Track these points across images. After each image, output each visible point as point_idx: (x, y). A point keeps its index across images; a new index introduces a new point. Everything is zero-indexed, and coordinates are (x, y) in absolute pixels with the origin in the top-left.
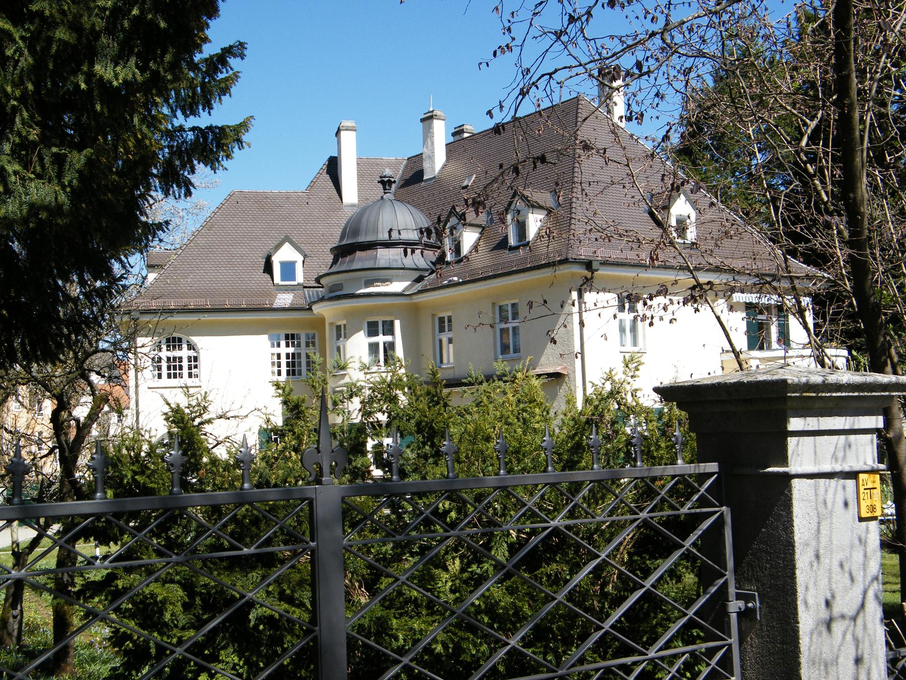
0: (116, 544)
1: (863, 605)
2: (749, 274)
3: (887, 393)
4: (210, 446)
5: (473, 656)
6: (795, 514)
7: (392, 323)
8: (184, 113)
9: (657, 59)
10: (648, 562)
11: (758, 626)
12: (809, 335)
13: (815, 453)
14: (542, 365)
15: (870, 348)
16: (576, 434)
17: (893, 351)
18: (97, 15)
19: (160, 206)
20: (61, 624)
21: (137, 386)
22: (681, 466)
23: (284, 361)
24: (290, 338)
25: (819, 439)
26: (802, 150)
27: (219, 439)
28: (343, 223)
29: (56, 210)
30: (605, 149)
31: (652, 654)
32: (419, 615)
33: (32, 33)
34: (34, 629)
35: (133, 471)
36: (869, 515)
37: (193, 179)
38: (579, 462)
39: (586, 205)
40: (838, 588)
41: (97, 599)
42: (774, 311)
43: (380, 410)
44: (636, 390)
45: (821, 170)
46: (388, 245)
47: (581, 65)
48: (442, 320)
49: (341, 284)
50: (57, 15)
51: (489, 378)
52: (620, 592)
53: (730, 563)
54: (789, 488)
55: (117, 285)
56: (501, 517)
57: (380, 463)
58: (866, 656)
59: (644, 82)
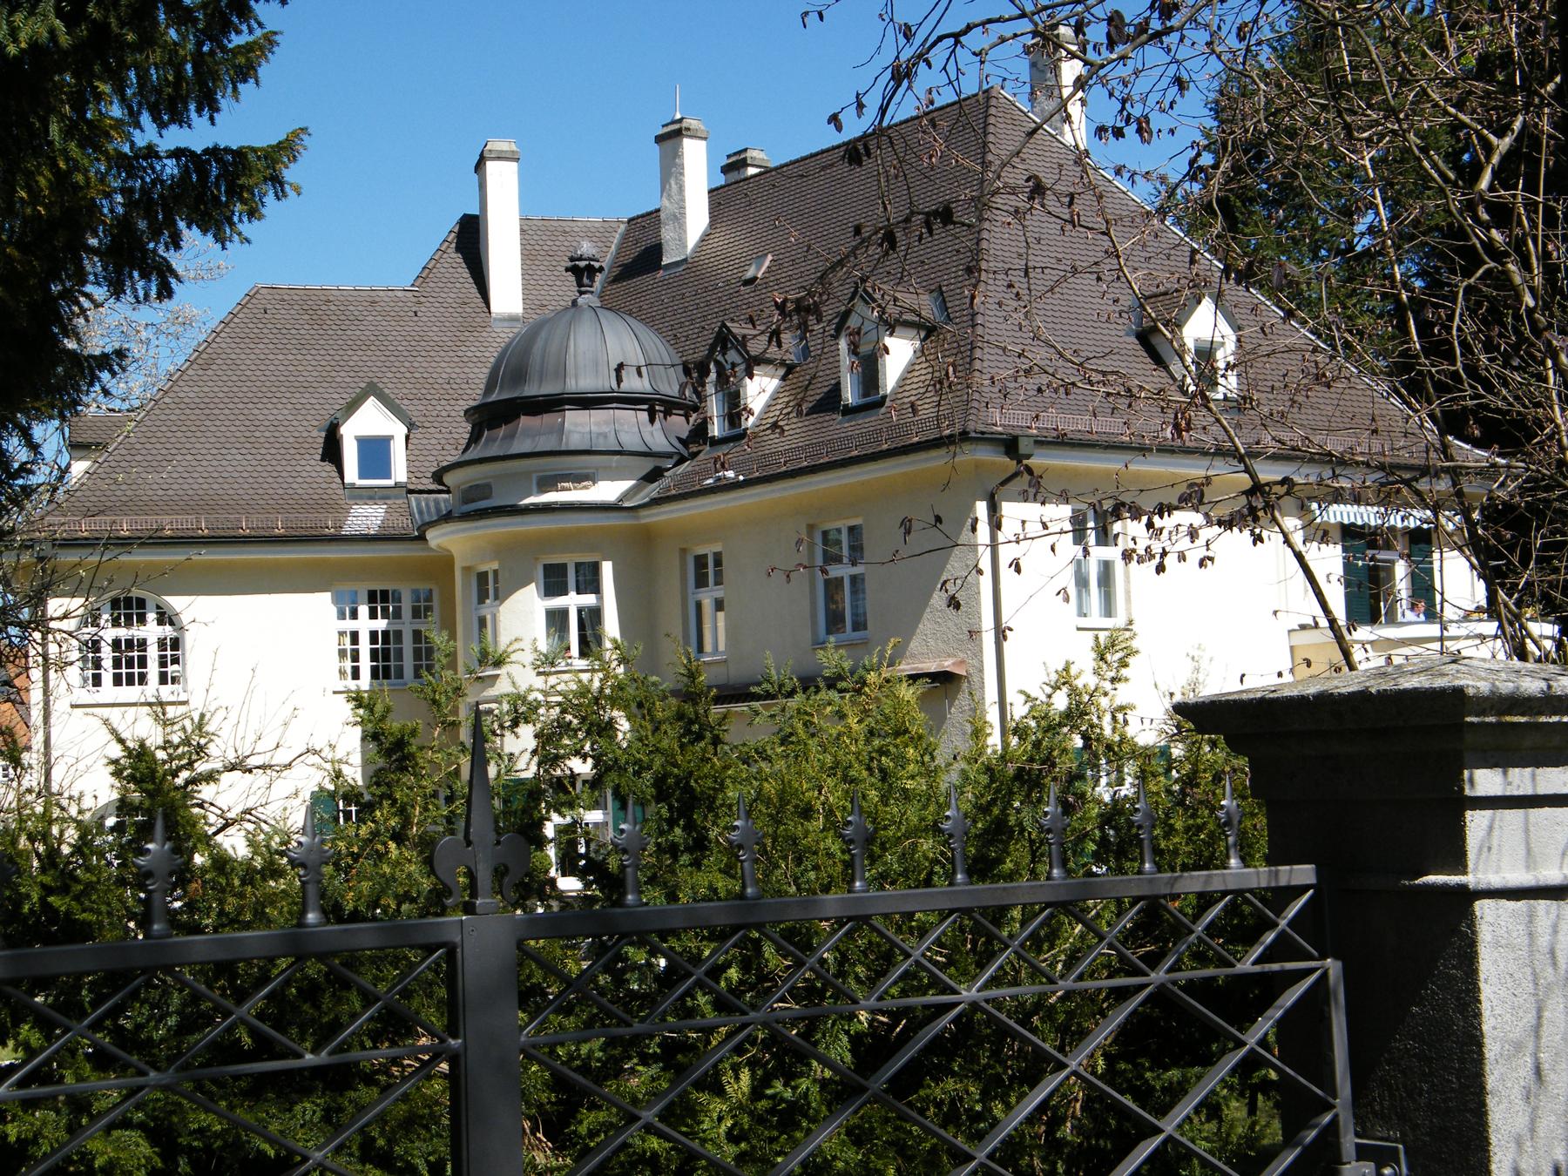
2: (1367, 465)
4: (211, 831)
6: (1482, 976)
7: (595, 569)
8: (156, 119)
10: (1148, 1075)
14: (913, 656)
16: (993, 802)
19: (104, 320)
22: (1235, 872)
23: (365, 647)
24: (379, 600)
25: (1537, 814)
26: (1483, 200)
27: (229, 815)
28: (491, 356)
30: (1072, 196)
35: (43, 886)
37: (176, 260)
43: (577, 753)
44: (1121, 708)
45: (1519, 246)
46: (587, 402)
47: (1023, 15)
48: (701, 562)
49: (488, 487)
51: (808, 683)
52: (1088, 1138)
54: (1469, 918)
55: (11, 486)
59: (1153, 54)
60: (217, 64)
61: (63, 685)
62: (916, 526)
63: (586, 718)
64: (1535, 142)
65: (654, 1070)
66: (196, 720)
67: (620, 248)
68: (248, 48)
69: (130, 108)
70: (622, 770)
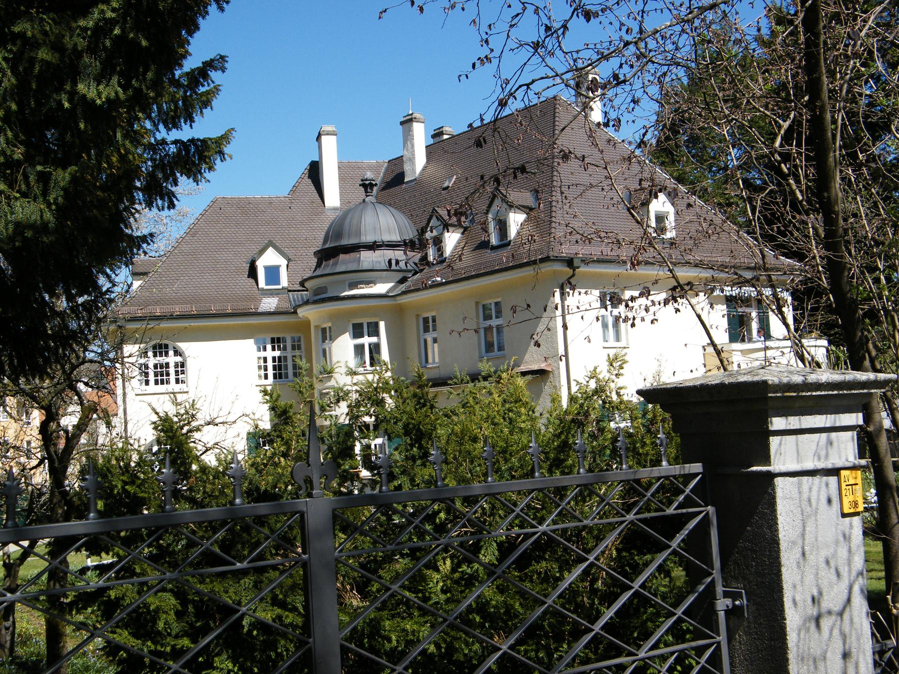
0: (108, 554)
1: (849, 600)
3: (865, 391)
5: (465, 655)
6: (778, 512)
7: (377, 325)
8: (166, 127)
9: (632, 66)
11: (745, 623)
12: (789, 331)
13: (798, 451)
14: (526, 362)
15: (851, 346)
16: (562, 433)
17: (871, 346)
18: (79, 35)
19: (145, 220)
20: (54, 635)
21: (124, 394)
23: (270, 364)
24: (276, 342)
25: (800, 437)
26: (776, 151)
27: (208, 446)
29: (42, 228)
31: (642, 654)
32: (411, 616)
33: (14, 54)
34: (26, 640)
35: (123, 481)
36: (852, 511)
38: (565, 460)
39: (566, 207)
40: (824, 584)
41: (90, 610)
42: (754, 303)
43: (367, 414)
44: (621, 388)
46: (373, 246)
47: (557, 75)
48: (426, 320)
49: (325, 287)
50: (39, 36)
51: (474, 378)
52: (609, 588)
53: (717, 563)
56: (489, 516)
57: (368, 464)
58: (854, 650)
60: (193, 100)
61: (130, 388)
62: (518, 309)
63: (371, 397)
64: (800, 124)
65: (407, 560)
66: (191, 402)
67: (385, 174)
68: (208, 93)
69: (154, 122)
70: (388, 422)
